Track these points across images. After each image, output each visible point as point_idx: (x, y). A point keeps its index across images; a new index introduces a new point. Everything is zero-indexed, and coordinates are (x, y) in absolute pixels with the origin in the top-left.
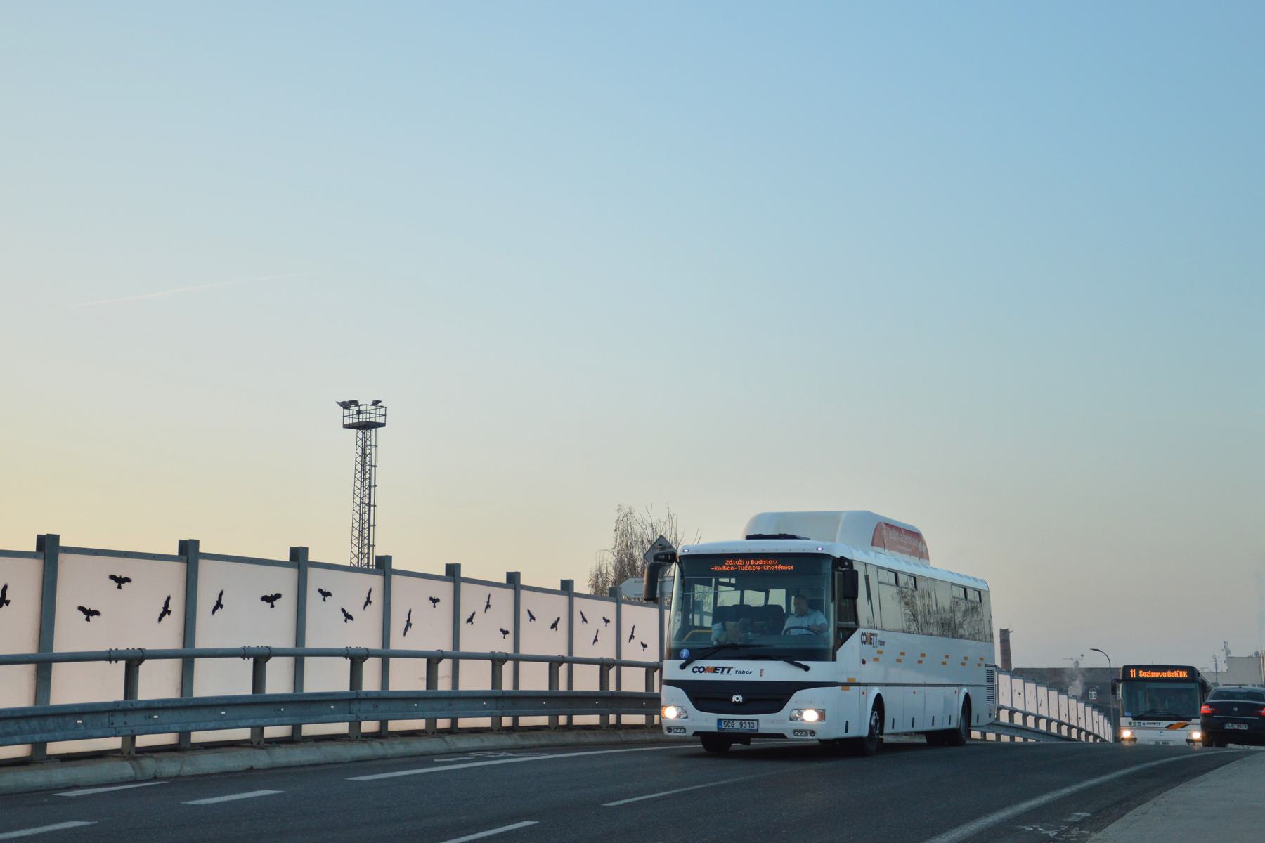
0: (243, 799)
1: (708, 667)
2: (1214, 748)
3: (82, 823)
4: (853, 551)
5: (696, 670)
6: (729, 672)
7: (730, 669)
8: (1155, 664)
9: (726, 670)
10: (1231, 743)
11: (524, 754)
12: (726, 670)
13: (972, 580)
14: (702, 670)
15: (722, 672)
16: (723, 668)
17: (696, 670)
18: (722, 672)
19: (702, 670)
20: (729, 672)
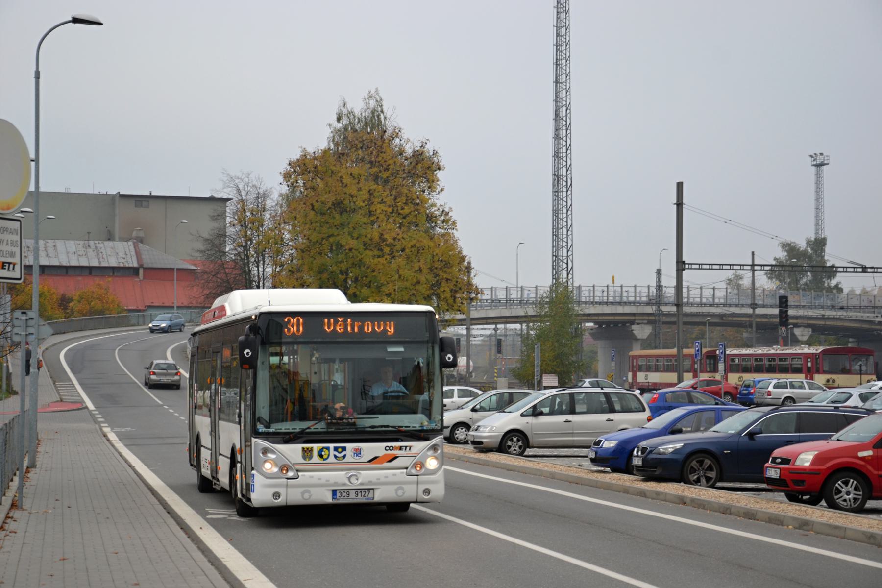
0: (618, 508)
1: (395, 446)
2: (288, 423)
3: (836, 347)
4: (816, 453)
5: (387, 448)
6: (410, 449)
7: (410, 447)
8: (51, 264)
9: (408, 448)
10: (641, 441)
11: (784, 366)
12: (408, 448)
13: (470, 447)
14: (391, 448)
15: (406, 449)
16: (406, 447)
17: (387, 448)
18: (406, 449)
19: (391, 448)
20: (410, 449)
